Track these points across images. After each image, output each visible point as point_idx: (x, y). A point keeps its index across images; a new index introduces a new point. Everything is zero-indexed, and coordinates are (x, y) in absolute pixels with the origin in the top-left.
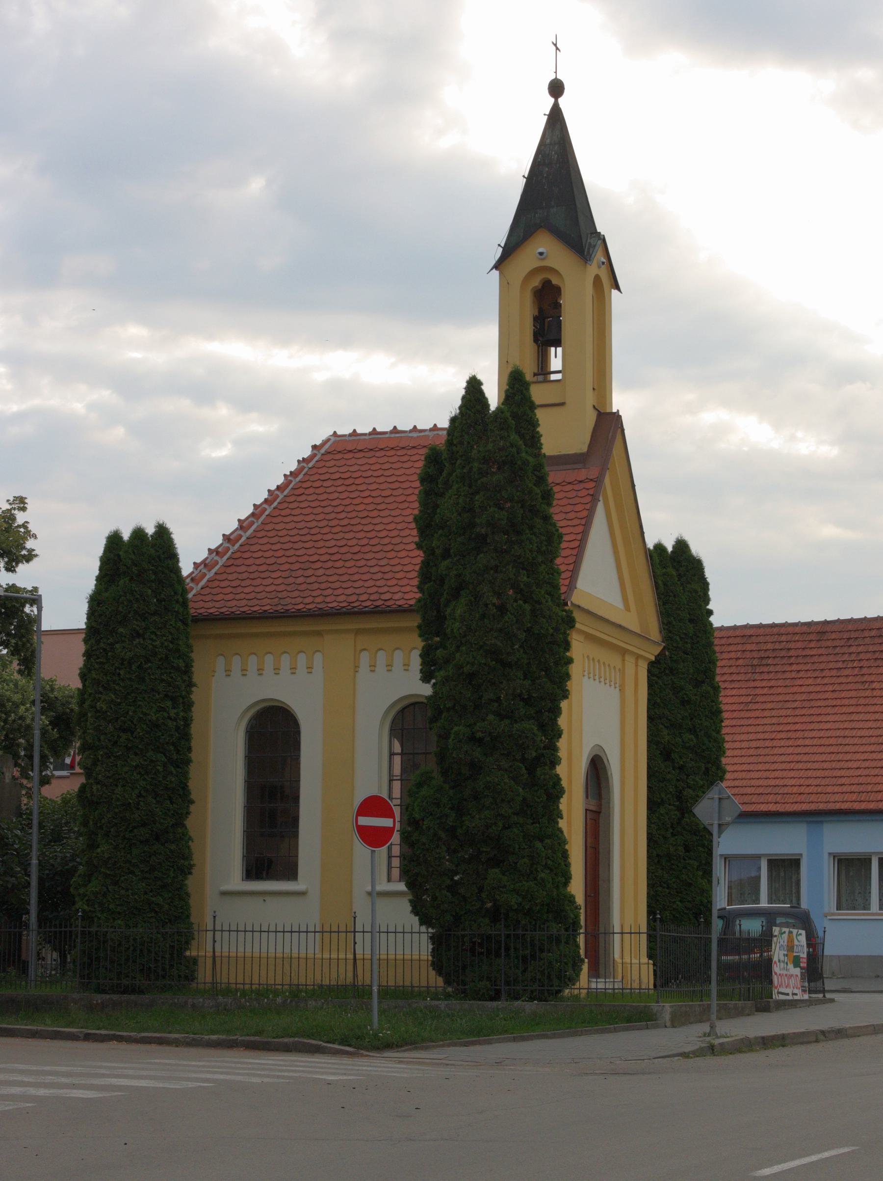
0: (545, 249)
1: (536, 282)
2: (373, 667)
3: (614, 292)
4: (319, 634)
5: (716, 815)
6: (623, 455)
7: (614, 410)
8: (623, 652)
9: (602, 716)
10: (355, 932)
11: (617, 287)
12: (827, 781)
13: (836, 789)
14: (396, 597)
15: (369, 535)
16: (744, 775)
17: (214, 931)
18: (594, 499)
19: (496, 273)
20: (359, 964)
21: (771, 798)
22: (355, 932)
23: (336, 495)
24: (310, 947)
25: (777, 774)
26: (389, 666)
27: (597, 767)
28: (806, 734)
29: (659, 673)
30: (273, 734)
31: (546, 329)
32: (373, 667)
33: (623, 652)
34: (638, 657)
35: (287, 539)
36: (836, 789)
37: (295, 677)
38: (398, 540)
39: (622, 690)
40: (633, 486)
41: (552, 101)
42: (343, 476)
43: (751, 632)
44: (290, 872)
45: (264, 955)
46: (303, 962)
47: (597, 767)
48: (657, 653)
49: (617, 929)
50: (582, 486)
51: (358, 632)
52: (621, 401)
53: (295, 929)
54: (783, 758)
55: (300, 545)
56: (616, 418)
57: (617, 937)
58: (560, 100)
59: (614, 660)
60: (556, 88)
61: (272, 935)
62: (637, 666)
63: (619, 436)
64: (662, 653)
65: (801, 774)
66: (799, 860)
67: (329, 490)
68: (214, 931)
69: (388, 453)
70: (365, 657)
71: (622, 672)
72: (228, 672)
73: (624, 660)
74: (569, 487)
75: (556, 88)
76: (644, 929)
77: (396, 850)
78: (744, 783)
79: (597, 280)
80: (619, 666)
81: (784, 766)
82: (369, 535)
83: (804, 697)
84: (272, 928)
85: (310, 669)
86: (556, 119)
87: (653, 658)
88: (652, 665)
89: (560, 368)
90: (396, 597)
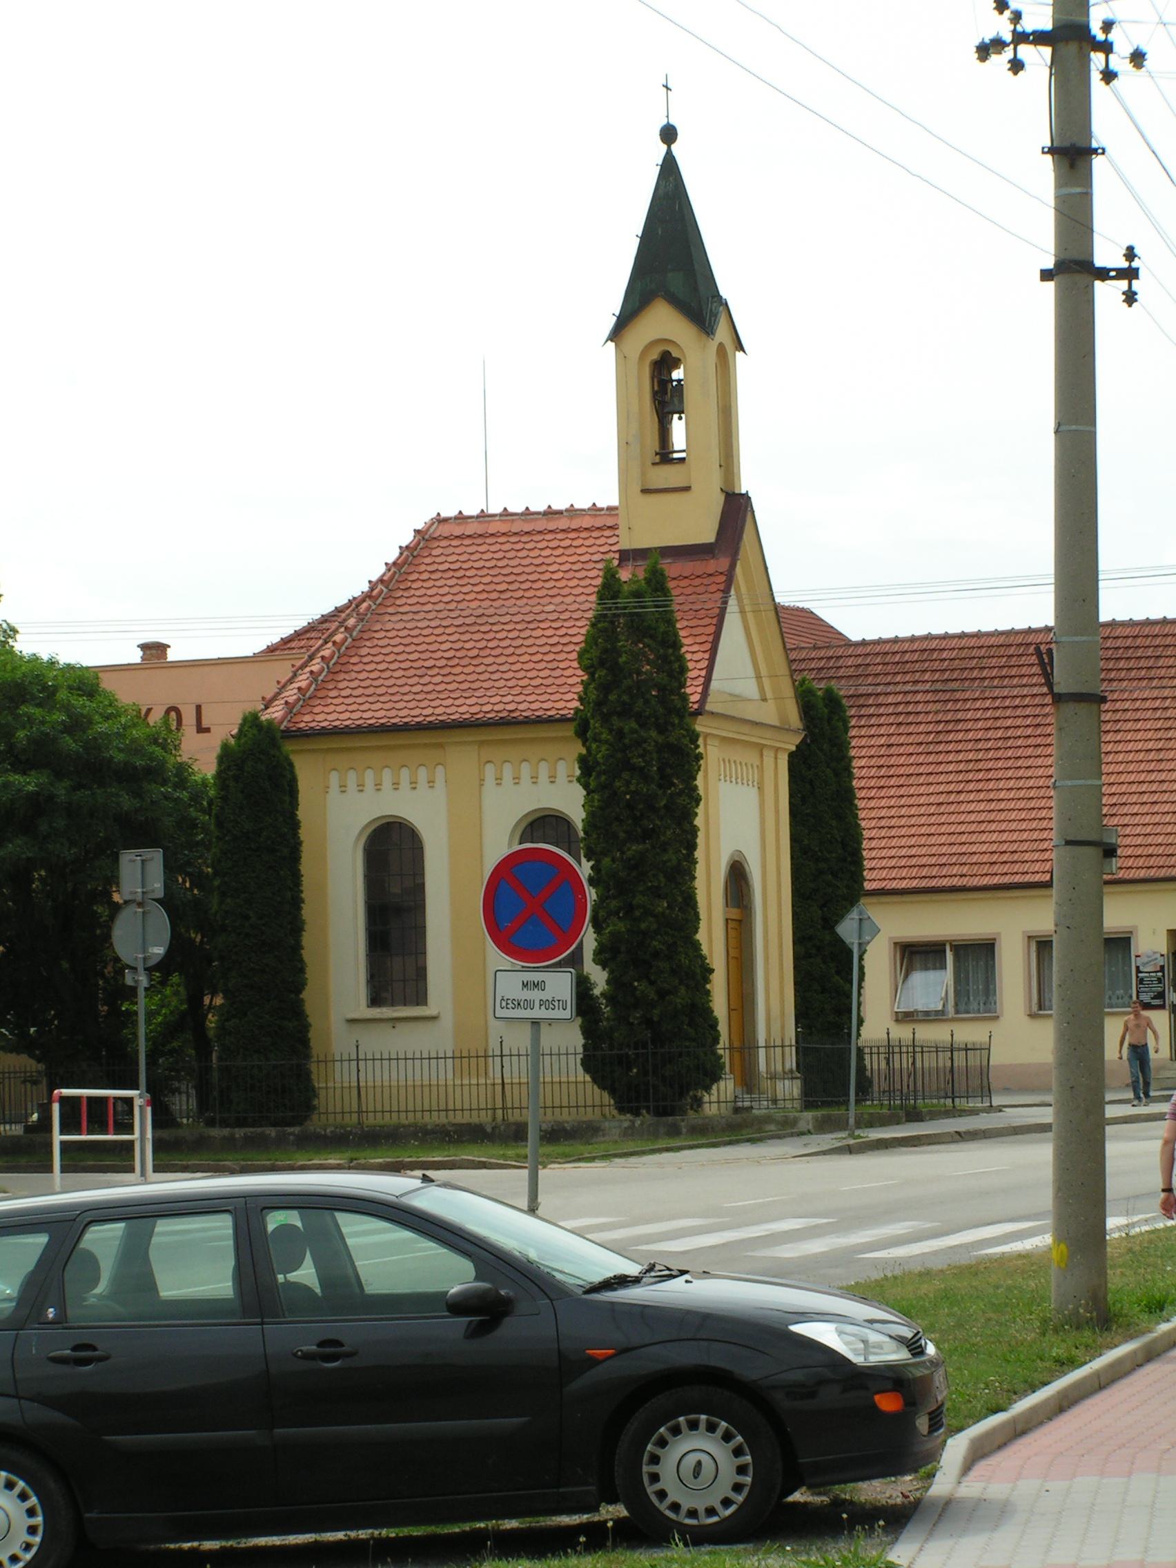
0: (663, 323)
1: (655, 355)
2: (499, 780)
3: (739, 355)
4: (440, 746)
5: (856, 935)
6: (754, 532)
7: (743, 491)
8: (761, 748)
9: (741, 818)
10: (502, 1056)
11: (740, 347)
12: (1025, 846)
13: (1036, 856)
14: (521, 707)
15: (487, 637)
16: (923, 840)
17: (358, 1060)
18: (726, 591)
19: (611, 345)
20: (508, 1087)
21: (955, 870)
22: (502, 1056)
23: (446, 589)
24: (445, 1073)
25: (963, 838)
26: (517, 780)
27: (737, 874)
28: (1001, 784)
29: (799, 763)
30: (392, 853)
31: (666, 399)
32: (499, 780)
33: (761, 748)
34: (777, 750)
35: (398, 640)
36: (1036, 856)
37: (418, 796)
38: (519, 642)
39: (760, 788)
40: (766, 568)
41: (665, 147)
42: (453, 567)
43: (934, 644)
44: (420, 998)
45: (386, 1084)
46: (426, 1090)
47: (737, 874)
48: (798, 742)
49: (762, 1042)
50: (712, 579)
51: (482, 743)
52: (747, 483)
53: (433, 1055)
54: (973, 817)
55: (413, 648)
56: (746, 498)
57: (762, 1052)
58: (673, 147)
59: (751, 757)
60: (669, 134)
61: (418, 1062)
62: (776, 758)
63: (749, 514)
64: (803, 741)
65: (994, 837)
66: (993, 945)
67: (438, 584)
68: (358, 1060)
69: (500, 540)
70: (490, 771)
71: (761, 768)
72: (343, 788)
73: (762, 755)
74: (698, 581)
75: (669, 134)
76: (794, 1043)
77: (1160, 1225)
78: (924, 851)
79: (721, 348)
80: (757, 762)
81: (973, 827)
82: (487, 637)
83: (1000, 734)
84: (386, 1056)
85: (431, 782)
86: (669, 168)
87: (794, 748)
88: (792, 755)
89: (684, 447)
90: (521, 707)
